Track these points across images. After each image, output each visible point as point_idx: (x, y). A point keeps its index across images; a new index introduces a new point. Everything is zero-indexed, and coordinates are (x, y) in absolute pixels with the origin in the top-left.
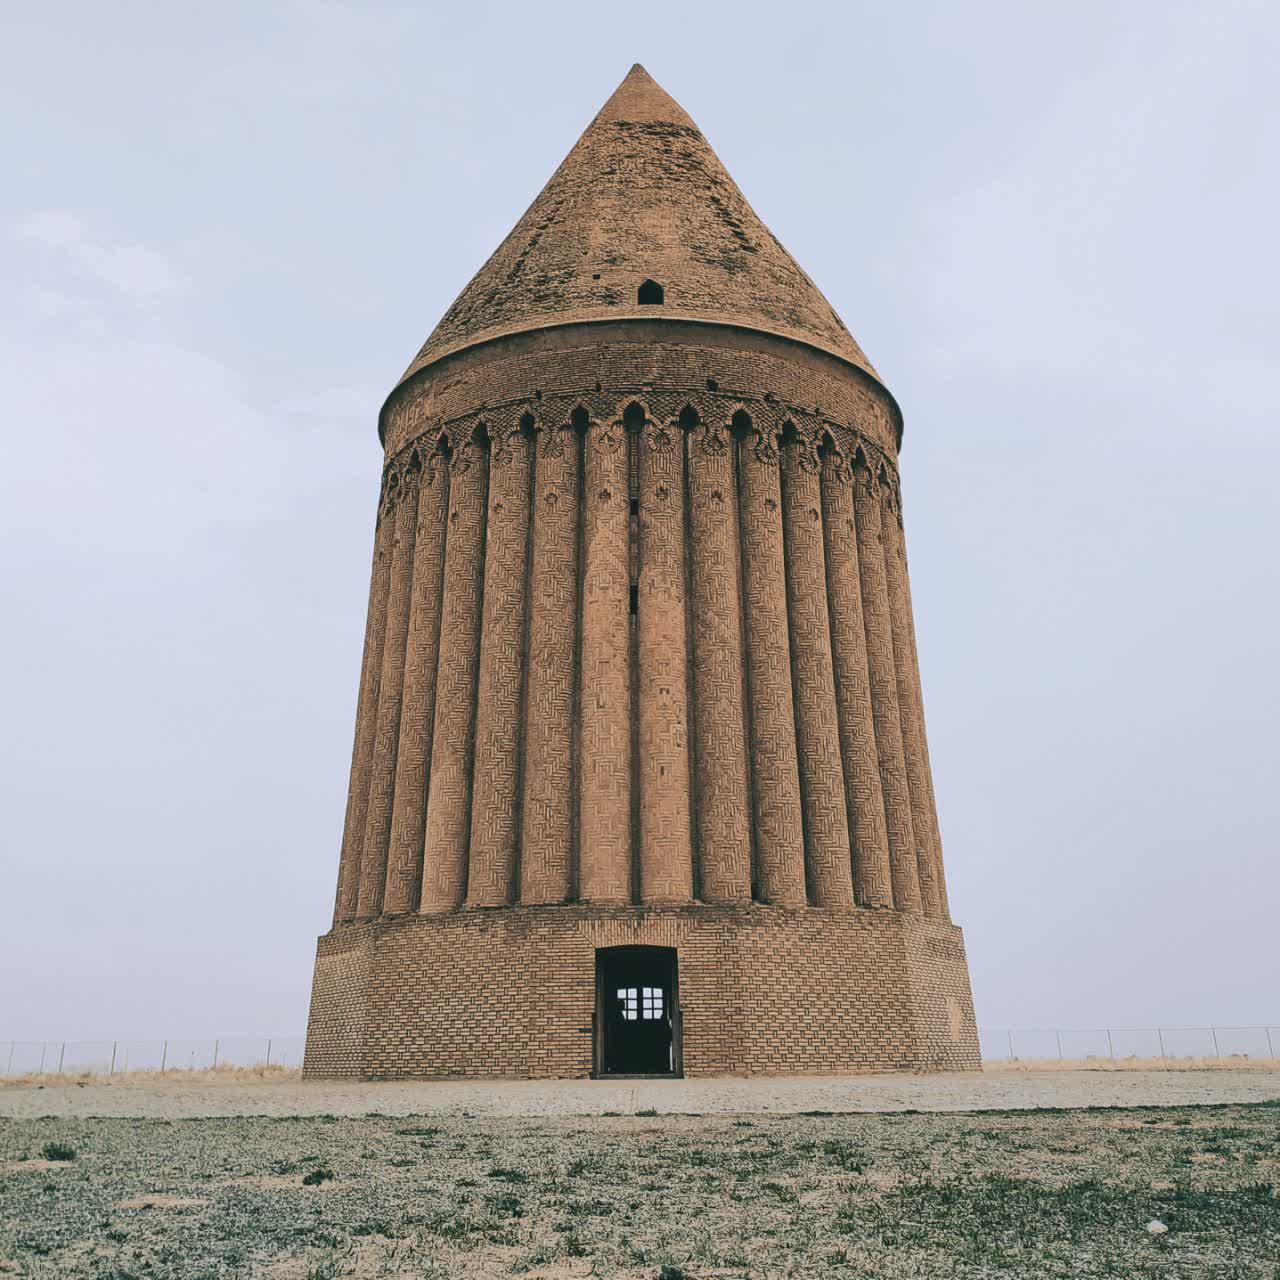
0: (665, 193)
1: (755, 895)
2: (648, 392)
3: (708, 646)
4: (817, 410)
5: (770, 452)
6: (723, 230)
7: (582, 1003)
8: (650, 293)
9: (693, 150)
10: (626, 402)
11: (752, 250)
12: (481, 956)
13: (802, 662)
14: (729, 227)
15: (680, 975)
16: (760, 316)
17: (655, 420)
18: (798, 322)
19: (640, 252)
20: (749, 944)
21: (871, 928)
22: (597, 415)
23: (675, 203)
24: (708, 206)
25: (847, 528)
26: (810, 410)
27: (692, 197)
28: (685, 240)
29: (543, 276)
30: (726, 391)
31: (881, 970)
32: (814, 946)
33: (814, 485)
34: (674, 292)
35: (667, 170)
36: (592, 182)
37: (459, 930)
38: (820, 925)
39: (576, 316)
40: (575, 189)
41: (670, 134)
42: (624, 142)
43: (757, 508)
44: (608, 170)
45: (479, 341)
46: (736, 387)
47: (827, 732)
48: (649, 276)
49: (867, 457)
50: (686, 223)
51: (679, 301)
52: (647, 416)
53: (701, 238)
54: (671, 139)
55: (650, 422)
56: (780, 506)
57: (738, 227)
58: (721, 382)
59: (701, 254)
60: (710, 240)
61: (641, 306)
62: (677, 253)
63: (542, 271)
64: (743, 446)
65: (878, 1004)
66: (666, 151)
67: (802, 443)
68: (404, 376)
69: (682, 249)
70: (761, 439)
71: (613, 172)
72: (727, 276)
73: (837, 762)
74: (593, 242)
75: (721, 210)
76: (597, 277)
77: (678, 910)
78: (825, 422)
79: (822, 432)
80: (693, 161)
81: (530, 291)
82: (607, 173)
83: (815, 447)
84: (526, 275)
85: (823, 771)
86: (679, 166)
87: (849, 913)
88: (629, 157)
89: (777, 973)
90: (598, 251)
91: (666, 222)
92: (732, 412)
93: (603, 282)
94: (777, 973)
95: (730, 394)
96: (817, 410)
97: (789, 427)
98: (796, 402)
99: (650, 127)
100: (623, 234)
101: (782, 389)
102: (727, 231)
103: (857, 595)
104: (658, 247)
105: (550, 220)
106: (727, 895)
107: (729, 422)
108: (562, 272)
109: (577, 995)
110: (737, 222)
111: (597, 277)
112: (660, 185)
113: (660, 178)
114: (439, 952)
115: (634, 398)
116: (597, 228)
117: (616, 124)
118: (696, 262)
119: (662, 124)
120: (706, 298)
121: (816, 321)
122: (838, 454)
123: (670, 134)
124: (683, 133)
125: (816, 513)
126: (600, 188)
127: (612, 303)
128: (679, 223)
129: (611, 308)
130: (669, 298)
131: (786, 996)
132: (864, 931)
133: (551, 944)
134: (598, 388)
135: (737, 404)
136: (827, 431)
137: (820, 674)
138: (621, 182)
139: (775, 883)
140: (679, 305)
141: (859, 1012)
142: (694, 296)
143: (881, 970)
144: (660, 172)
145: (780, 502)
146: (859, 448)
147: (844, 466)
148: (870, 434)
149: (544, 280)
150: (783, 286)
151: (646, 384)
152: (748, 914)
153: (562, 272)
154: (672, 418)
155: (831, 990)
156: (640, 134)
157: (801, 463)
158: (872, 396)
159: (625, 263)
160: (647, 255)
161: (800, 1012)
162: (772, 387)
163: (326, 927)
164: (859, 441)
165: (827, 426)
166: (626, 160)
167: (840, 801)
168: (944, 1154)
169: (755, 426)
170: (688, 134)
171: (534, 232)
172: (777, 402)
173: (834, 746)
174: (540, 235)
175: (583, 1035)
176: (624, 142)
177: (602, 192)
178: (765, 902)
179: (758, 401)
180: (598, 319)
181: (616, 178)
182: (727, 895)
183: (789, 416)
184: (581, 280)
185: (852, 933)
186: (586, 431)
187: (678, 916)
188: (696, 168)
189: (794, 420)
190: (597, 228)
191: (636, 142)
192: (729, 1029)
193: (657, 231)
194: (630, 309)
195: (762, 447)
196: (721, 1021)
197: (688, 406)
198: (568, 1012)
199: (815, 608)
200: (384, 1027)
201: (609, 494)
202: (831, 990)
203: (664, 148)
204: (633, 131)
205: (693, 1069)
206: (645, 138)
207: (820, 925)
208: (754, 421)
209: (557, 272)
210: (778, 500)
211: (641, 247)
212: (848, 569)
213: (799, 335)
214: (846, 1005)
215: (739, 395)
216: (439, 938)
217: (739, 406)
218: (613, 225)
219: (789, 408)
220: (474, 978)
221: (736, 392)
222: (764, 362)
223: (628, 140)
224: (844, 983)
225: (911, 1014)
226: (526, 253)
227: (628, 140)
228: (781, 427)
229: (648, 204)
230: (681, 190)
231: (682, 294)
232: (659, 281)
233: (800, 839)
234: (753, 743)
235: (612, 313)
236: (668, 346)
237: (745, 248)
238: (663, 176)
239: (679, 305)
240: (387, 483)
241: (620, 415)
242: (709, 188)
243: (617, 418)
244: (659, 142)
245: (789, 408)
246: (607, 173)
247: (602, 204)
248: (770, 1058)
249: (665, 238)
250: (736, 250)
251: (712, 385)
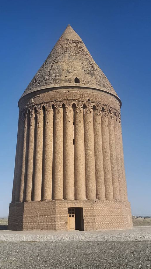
0: (78, 57)
3: (89, 151)
11: (96, 71)
16: (98, 86)
17: (78, 107)
25: (113, 128)
28: (83, 68)
32: (107, 207)
35: (78, 52)
38: (108, 203)
41: (77, 42)
43: (97, 124)
47: (109, 167)
55: (77, 107)
57: (92, 65)
58: (91, 99)
62: (81, 72)
70: (98, 111)
73: (111, 173)
74: (64, 68)
78: (109, 107)
84: (51, 74)
93: (67, 78)
95: (92, 102)
96: (108, 105)
98: (104, 103)
101: (102, 100)
102: (90, 66)
107: (92, 108)
111: (66, 76)
115: (74, 102)
117: (66, 40)
119: (76, 40)
123: (77, 42)
124: (80, 42)
128: (81, 64)
130: (81, 81)
134: (67, 100)
137: (108, 156)
139: (100, 196)
143: (118, 211)
146: (115, 112)
148: (117, 109)
154: (82, 107)
157: (105, 115)
159: (71, 74)
161: (105, 219)
165: (110, 108)
167: (111, 180)
168: (66, 223)
177: (65, 56)
180: (67, 86)
183: (103, 106)
187: (83, 202)
191: (71, 44)
194: (73, 84)
197: (84, 104)
207: (108, 203)
210: (101, 123)
212: (113, 136)
217: (93, 104)
226: (50, 69)
229: (74, 59)
234: (96, 170)
236: (81, 92)
237: (94, 70)
248: (100, 227)
249: (79, 68)
251: (89, 100)
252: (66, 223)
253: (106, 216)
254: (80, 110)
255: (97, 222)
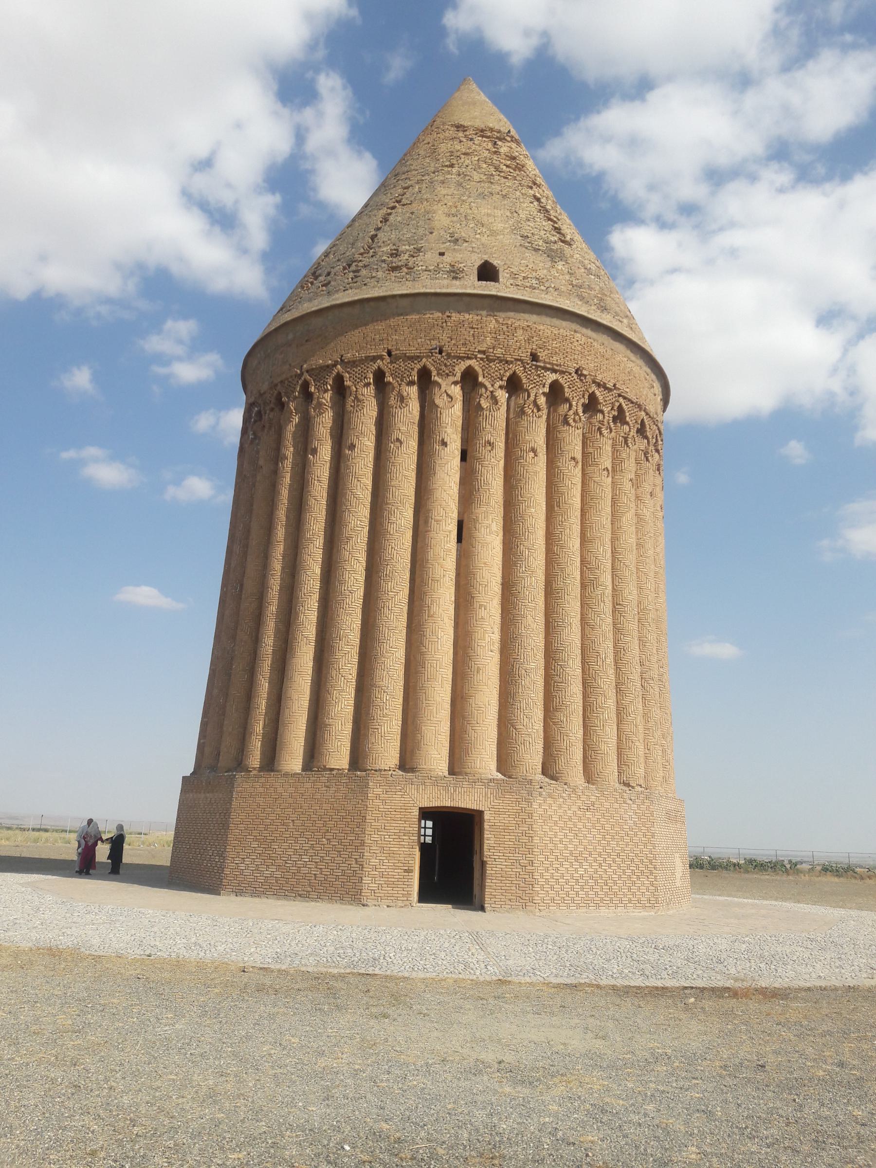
0: (496, 188)
1: (452, 771)
2: (482, 359)
4: (614, 385)
5: (577, 418)
6: (544, 223)
7: (407, 850)
8: (487, 272)
9: (517, 154)
10: (463, 366)
12: (325, 806)
13: (589, 589)
14: (549, 222)
15: (486, 832)
18: (604, 309)
19: (478, 236)
20: (541, 812)
21: (631, 802)
22: (438, 374)
23: (505, 197)
24: (532, 203)
26: (610, 385)
27: (518, 193)
28: (515, 229)
29: (395, 250)
30: (545, 362)
31: (636, 835)
33: (608, 448)
34: (507, 273)
35: (497, 169)
36: (434, 173)
37: (308, 785)
38: (593, 798)
39: (425, 287)
40: (419, 177)
41: (497, 138)
42: (461, 142)
44: (448, 163)
45: (338, 302)
46: (554, 360)
48: (486, 257)
49: (648, 427)
50: (515, 215)
51: (512, 281)
52: (481, 379)
53: (528, 228)
54: (499, 143)
56: (580, 464)
58: (542, 355)
59: (529, 243)
60: (536, 231)
61: (480, 282)
62: (508, 240)
63: (394, 245)
64: (555, 411)
65: (632, 861)
66: (495, 152)
67: (602, 412)
68: (263, 333)
69: (513, 236)
71: (452, 166)
72: (549, 264)
75: (542, 207)
76: (442, 254)
77: (486, 781)
78: (620, 395)
79: (617, 404)
80: (517, 164)
81: (384, 261)
82: (446, 166)
83: (611, 416)
85: (601, 678)
86: (507, 166)
87: (615, 790)
88: (464, 154)
89: (560, 835)
90: (442, 233)
91: (498, 213)
92: (549, 381)
93: (447, 258)
94: (560, 835)
95: (548, 366)
96: (614, 385)
97: (592, 397)
98: (599, 378)
99: (482, 131)
100: (463, 219)
101: (589, 366)
102: (548, 225)
103: (633, 540)
104: (493, 233)
105: (398, 202)
106: (525, 772)
107: (546, 390)
108: (412, 247)
109: (403, 843)
110: (555, 219)
111: (442, 254)
112: (492, 181)
113: (492, 175)
114: (291, 800)
115: (469, 362)
116: (440, 212)
118: (524, 249)
119: (492, 130)
120: (534, 281)
121: (618, 309)
122: (627, 423)
125: (608, 470)
126: (441, 178)
127: (455, 278)
129: (454, 282)
130: (503, 276)
131: (566, 853)
132: (625, 805)
133: (384, 802)
135: (554, 374)
136: (620, 404)
138: (459, 175)
139: (562, 762)
140: (511, 285)
141: (619, 867)
142: (524, 278)
143: (636, 835)
144: (492, 169)
145: (581, 460)
147: (632, 434)
149: (395, 254)
150: (593, 277)
151: (479, 352)
152: (541, 788)
153: (412, 247)
155: (600, 849)
156: (474, 136)
158: (653, 377)
159: (465, 244)
160: (484, 239)
162: (582, 363)
163: (189, 770)
164: (643, 413)
165: (621, 400)
166: (463, 156)
167: (611, 703)
168: (405, 871)
169: (567, 395)
170: (512, 141)
171: (384, 211)
172: (585, 376)
173: (610, 660)
174: (390, 214)
175: (407, 874)
176: (461, 142)
177: (443, 182)
178: (552, 778)
179: (570, 374)
180: (444, 291)
181: (454, 170)
182: (525, 772)
183: (594, 388)
184: (429, 255)
185: (616, 805)
186: (428, 388)
188: (520, 170)
189: (598, 393)
190: (440, 212)
191: (470, 143)
192: (523, 876)
193: (491, 220)
194: (472, 285)
195: (571, 412)
196: (517, 870)
197: (514, 373)
198: (395, 855)
199: (603, 552)
200: (243, 855)
201: (446, 443)
202: (600, 849)
203: (494, 150)
204: (468, 133)
205: (492, 905)
206: (478, 140)
208: (566, 390)
209: (407, 247)
210: (579, 457)
211: (479, 231)
212: (628, 519)
213: (605, 319)
214: (609, 861)
215: (556, 367)
216: (291, 790)
217: (553, 377)
218: (454, 211)
219: (594, 382)
220: (320, 824)
221: (553, 364)
222: (577, 341)
223: (464, 140)
224: (608, 844)
225: (655, 868)
226: (378, 229)
227: (464, 140)
228: (586, 397)
230: (509, 187)
231: (514, 276)
232: (495, 263)
233: (581, 732)
234: (551, 655)
235: (456, 287)
237: (563, 242)
238: (494, 173)
239: (511, 285)
240: (250, 417)
241: (458, 377)
242: (531, 188)
243: (456, 379)
244: (490, 144)
245: (594, 382)
246: (446, 166)
247: (444, 192)
250: (555, 242)
251: (534, 357)
252: (405, 871)
253: (581, 853)
254: (448, 395)
255: (542, 875)
